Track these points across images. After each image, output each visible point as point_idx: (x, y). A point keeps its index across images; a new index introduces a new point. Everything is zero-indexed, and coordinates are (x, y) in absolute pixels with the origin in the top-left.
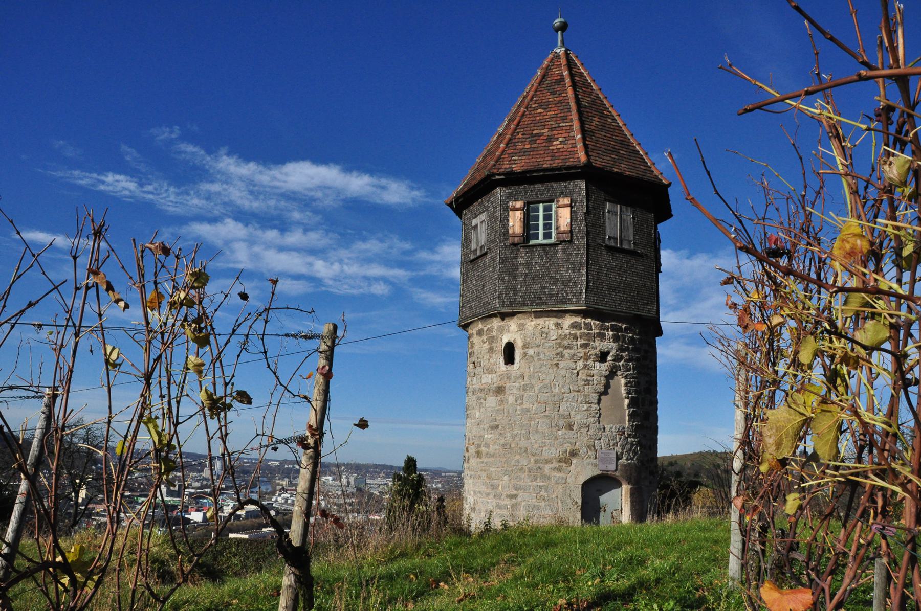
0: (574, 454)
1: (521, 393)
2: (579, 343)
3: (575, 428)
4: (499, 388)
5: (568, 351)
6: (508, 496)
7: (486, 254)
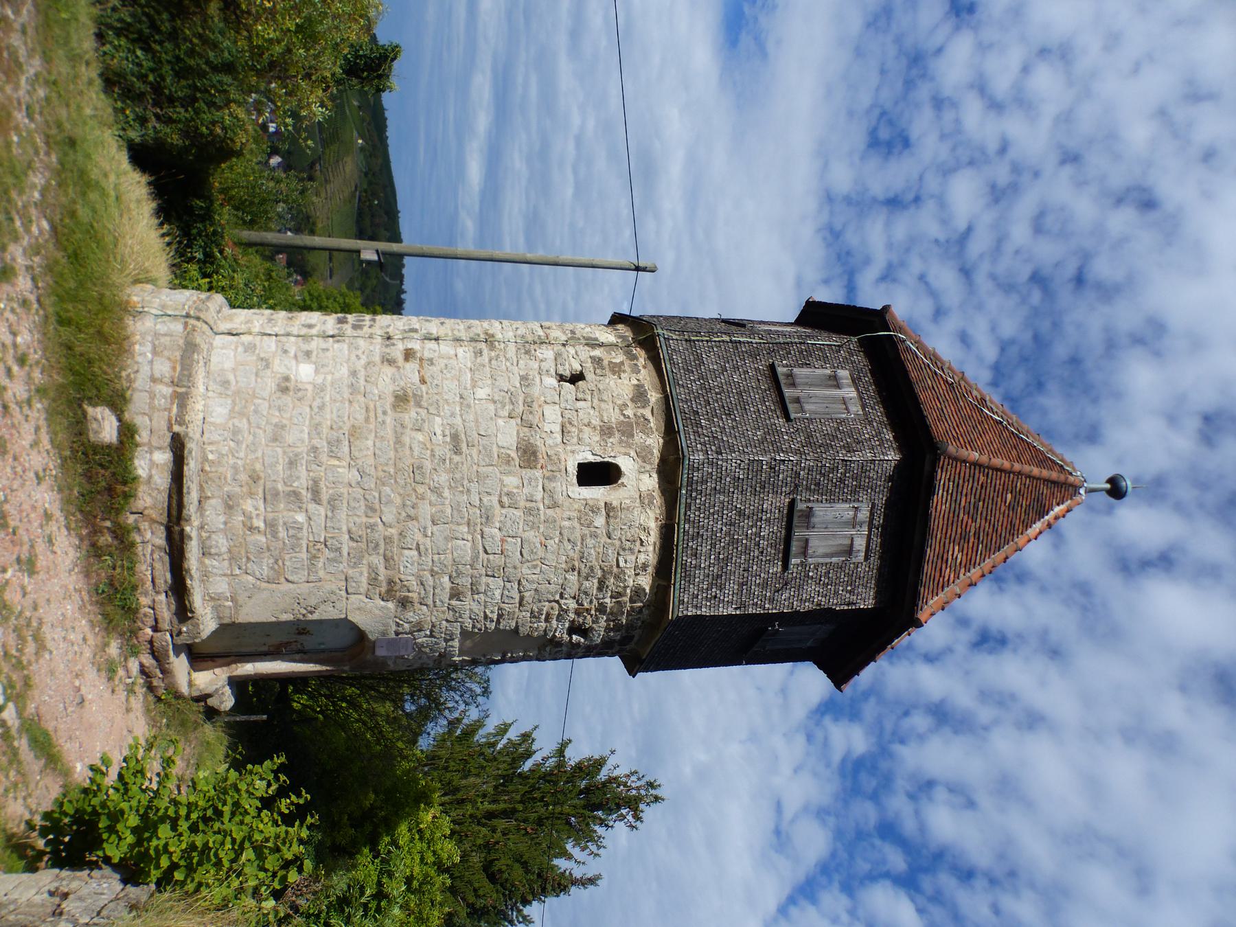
0: (404, 603)
1: (522, 504)
2: (608, 600)
3: (454, 602)
4: (534, 453)
5: (596, 585)
6: (316, 482)
7: (787, 418)
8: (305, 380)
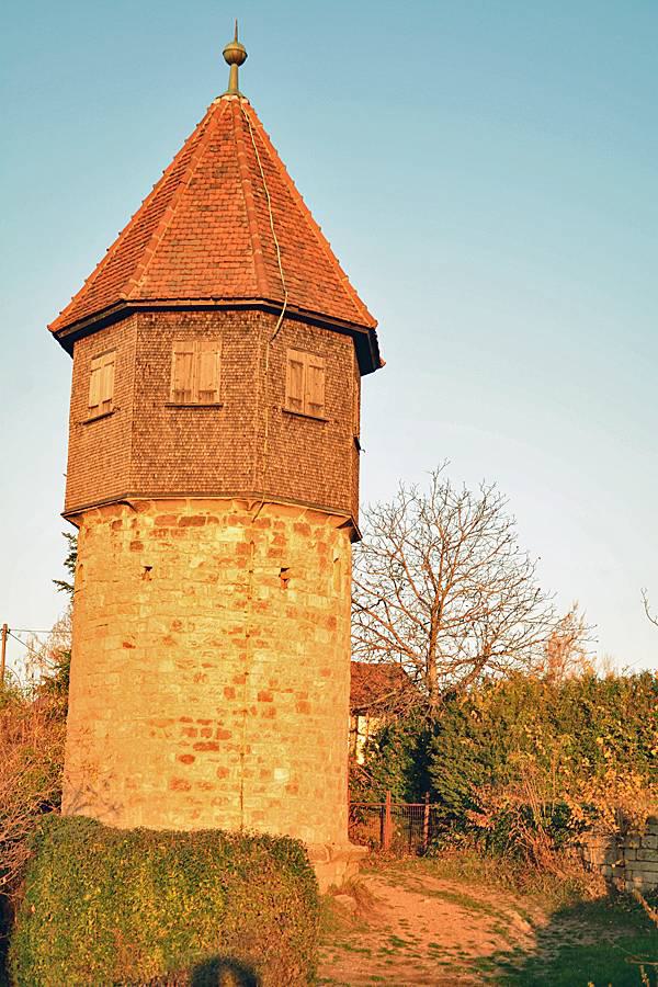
8: (287, 775)
